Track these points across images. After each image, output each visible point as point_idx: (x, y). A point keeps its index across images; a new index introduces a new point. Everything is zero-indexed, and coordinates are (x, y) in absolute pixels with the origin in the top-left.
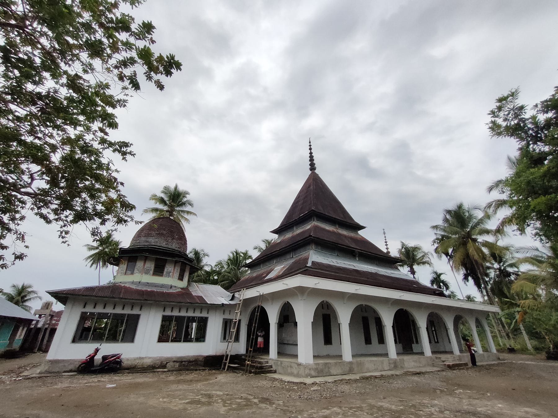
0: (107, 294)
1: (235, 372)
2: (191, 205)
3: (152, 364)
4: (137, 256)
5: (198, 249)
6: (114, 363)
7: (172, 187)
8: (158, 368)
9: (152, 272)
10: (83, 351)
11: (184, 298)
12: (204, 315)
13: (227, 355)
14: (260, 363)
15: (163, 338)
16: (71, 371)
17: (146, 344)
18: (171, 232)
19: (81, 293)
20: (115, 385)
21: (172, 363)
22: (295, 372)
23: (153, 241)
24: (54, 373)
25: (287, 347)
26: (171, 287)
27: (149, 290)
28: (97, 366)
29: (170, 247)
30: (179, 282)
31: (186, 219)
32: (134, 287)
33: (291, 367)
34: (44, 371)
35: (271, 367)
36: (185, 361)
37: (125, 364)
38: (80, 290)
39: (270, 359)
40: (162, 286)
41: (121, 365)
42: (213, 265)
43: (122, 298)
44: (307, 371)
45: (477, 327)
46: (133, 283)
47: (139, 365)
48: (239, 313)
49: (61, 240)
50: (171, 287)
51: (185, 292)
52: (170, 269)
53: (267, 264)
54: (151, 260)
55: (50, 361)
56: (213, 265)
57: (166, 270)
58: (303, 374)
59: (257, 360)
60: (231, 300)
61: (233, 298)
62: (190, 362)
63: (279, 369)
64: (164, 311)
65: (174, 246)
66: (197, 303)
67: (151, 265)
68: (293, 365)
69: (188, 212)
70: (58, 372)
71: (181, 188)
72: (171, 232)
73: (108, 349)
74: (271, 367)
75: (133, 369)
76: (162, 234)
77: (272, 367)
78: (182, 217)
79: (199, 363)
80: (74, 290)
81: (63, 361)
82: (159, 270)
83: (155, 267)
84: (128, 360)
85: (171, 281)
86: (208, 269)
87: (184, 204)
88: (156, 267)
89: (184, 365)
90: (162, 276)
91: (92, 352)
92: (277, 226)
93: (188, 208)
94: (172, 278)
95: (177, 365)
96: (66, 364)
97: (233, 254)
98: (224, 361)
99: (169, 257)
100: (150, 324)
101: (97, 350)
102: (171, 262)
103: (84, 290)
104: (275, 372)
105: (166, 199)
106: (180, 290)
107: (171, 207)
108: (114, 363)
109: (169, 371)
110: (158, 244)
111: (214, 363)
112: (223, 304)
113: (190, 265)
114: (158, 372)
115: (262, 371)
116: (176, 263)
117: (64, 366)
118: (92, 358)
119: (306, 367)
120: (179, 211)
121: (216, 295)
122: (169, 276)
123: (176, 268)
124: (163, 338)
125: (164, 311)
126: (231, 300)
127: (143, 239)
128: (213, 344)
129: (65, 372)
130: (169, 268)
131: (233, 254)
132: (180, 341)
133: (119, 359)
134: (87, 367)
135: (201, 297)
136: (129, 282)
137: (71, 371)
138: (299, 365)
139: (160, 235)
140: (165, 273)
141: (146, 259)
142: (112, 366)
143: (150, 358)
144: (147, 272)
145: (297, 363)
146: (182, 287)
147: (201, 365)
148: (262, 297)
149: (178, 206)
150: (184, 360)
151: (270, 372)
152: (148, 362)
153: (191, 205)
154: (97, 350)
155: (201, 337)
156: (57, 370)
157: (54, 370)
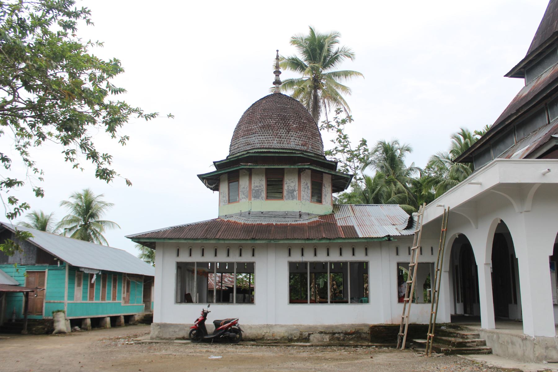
0: (199, 235)
1: (417, 351)
2: (350, 56)
3: (286, 334)
4: (237, 171)
5: (388, 141)
6: (230, 331)
7: (306, 34)
8: (298, 340)
9: (264, 194)
10: (189, 315)
11: (324, 230)
12: (360, 257)
13: (404, 326)
14: (463, 337)
15: (297, 295)
16: (184, 338)
17: (271, 306)
18: (284, 118)
19: (165, 236)
20: (220, 357)
21: (318, 336)
22: (520, 353)
23: (257, 141)
24: (164, 339)
25: (507, 306)
26: (300, 215)
27: (264, 223)
28: (210, 335)
29: (286, 146)
30: (318, 205)
31: (344, 88)
32: (242, 221)
33: (513, 343)
34: (155, 336)
35: (484, 343)
36: (339, 333)
37: (246, 332)
38: (165, 231)
39: (482, 330)
40: (285, 215)
41: (241, 335)
42: (423, 167)
43: (219, 239)
44: (540, 351)
45: (430, 199)
46: (241, 214)
47: (268, 336)
48: (417, 251)
49: (70, 164)
50: (300, 215)
51: (327, 222)
52: (292, 185)
53: (501, 147)
54: (258, 172)
55: (158, 325)
56: (423, 167)
57: (285, 187)
58: (531, 356)
59: (459, 332)
60: (407, 228)
61: (411, 224)
62: (346, 334)
63: (496, 349)
64: (290, 255)
65: (293, 142)
66: (341, 238)
67: (260, 183)
68: (515, 339)
69: (346, 74)
70: (170, 339)
71: (322, 31)
72: (284, 118)
73: (219, 312)
74: (484, 343)
75: (258, 341)
76: (269, 126)
77: (485, 344)
78: (337, 85)
79: (364, 335)
80: (158, 232)
81: (171, 325)
82: (275, 188)
83: (268, 185)
84: (251, 328)
85: (297, 204)
86: (416, 176)
87: (335, 58)
88: (269, 185)
89: (338, 339)
90: (282, 198)
91: (199, 316)
92: (519, 52)
93: (338, 67)
94: (299, 199)
95: (327, 338)
96: (177, 330)
97: (458, 139)
98: (400, 333)
99: (286, 164)
100: (272, 277)
101: (205, 314)
102: (291, 171)
103: (171, 232)
104: (490, 352)
105: (301, 57)
106: (317, 219)
107: (314, 70)
108: (230, 331)
109: (312, 346)
110: (266, 145)
111: (384, 336)
112: (389, 236)
113: (323, 174)
114: (294, 346)
115: (463, 348)
116: (300, 172)
117: (175, 332)
118: (201, 323)
119: (536, 342)
120: (329, 76)
121: (385, 221)
122: (293, 198)
123: (303, 181)
124: (297, 295)
125: (290, 255)
126: (407, 228)
127: (242, 140)
128: (382, 306)
129: (177, 339)
130: (290, 183)
131: (458, 139)
132: (347, 302)
133: (235, 325)
134: (199, 334)
135: (352, 228)
136: (236, 214)
137: (184, 338)
138: (525, 339)
139: (266, 127)
140: (285, 193)
141: (250, 173)
142: (229, 334)
143: (282, 326)
144: (257, 196)
145: (520, 337)
146: (322, 213)
147: (365, 339)
148: (450, 216)
149: (325, 66)
150: (336, 331)
151: (478, 352)
152: (280, 332)
153: (350, 56)
154: (205, 314)
155: (361, 295)
156: (168, 336)
157: (164, 336)
